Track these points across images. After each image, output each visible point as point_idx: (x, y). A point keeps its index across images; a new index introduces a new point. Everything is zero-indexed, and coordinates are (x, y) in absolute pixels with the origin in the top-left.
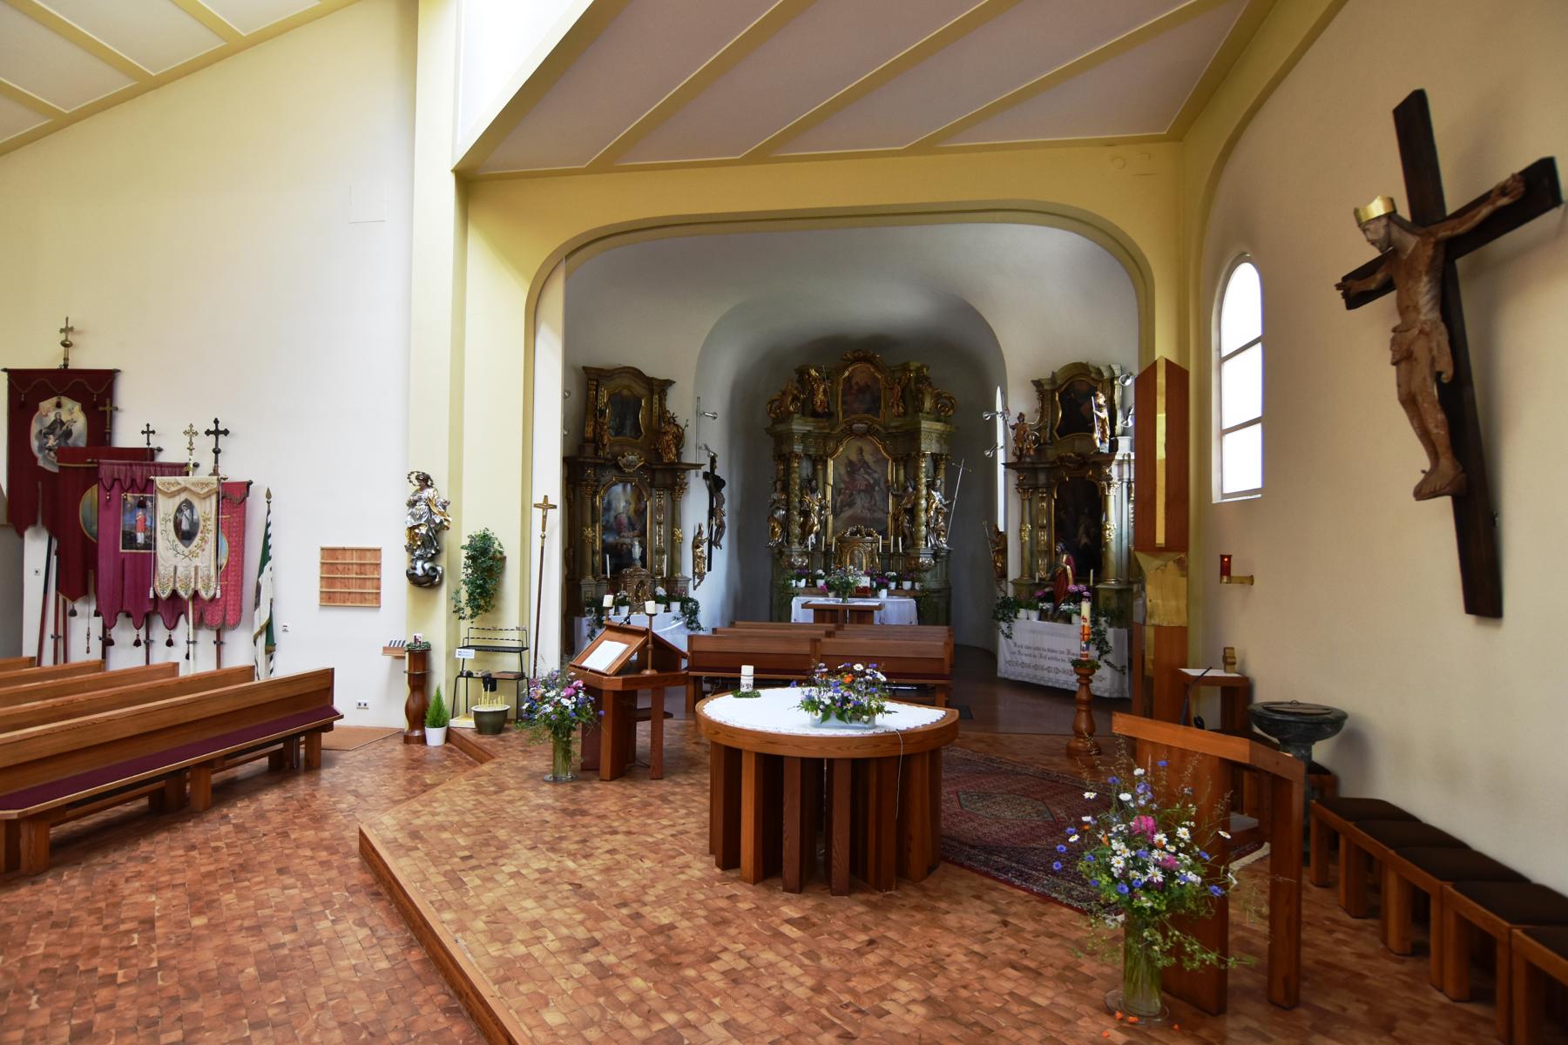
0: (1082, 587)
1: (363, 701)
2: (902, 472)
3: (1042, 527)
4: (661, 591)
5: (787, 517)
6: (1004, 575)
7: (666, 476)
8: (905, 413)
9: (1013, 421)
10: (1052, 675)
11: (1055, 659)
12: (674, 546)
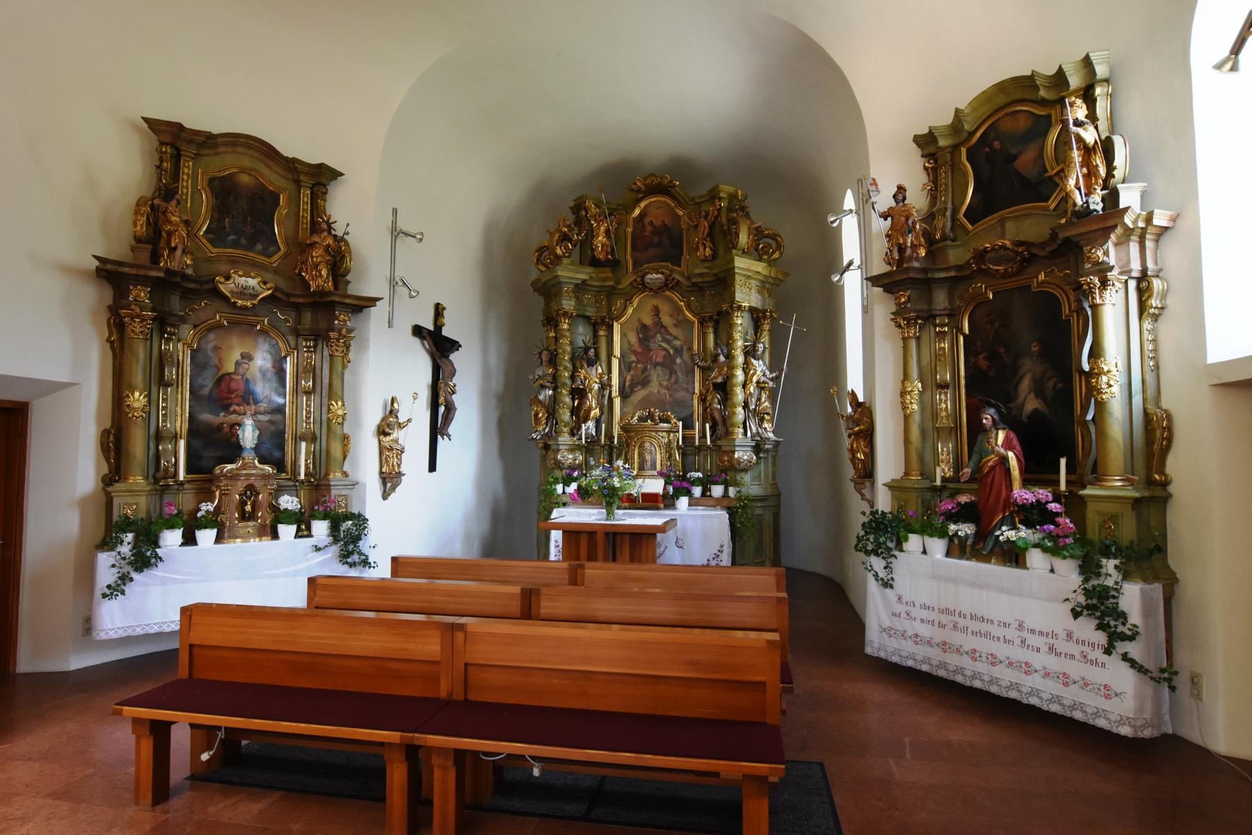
0: (1043, 494)
2: (711, 338)
3: (943, 386)
5: (555, 399)
6: (867, 473)
7: (321, 309)
8: (714, 256)
9: (884, 200)
10: (981, 667)
11: (987, 635)
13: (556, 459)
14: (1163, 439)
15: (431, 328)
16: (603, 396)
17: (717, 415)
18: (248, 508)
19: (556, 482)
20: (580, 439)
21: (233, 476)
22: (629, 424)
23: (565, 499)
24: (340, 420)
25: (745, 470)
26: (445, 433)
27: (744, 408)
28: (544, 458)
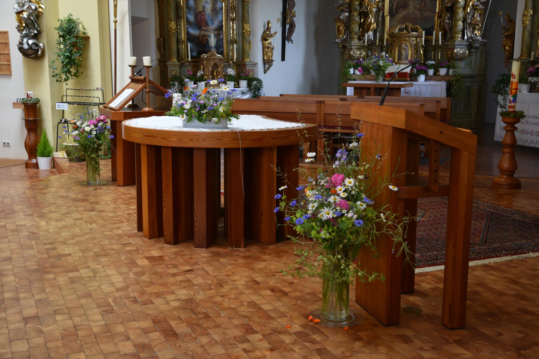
1: (6, 141)
4: (231, 72)
12: (244, 38)
13: (350, 54)
14: (179, 29)
15: (506, 125)
16: (379, 16)
17: (446, 27)
18: (215, 74)
19: (350, 67)
20: (364, 42)
21: (208, 60)
22: (393, 33)
23: (354, 77)
24: (248, 33)
25: (461, 59)
26: (290, 40)
27: (463, 22)
28: (343, 54)
